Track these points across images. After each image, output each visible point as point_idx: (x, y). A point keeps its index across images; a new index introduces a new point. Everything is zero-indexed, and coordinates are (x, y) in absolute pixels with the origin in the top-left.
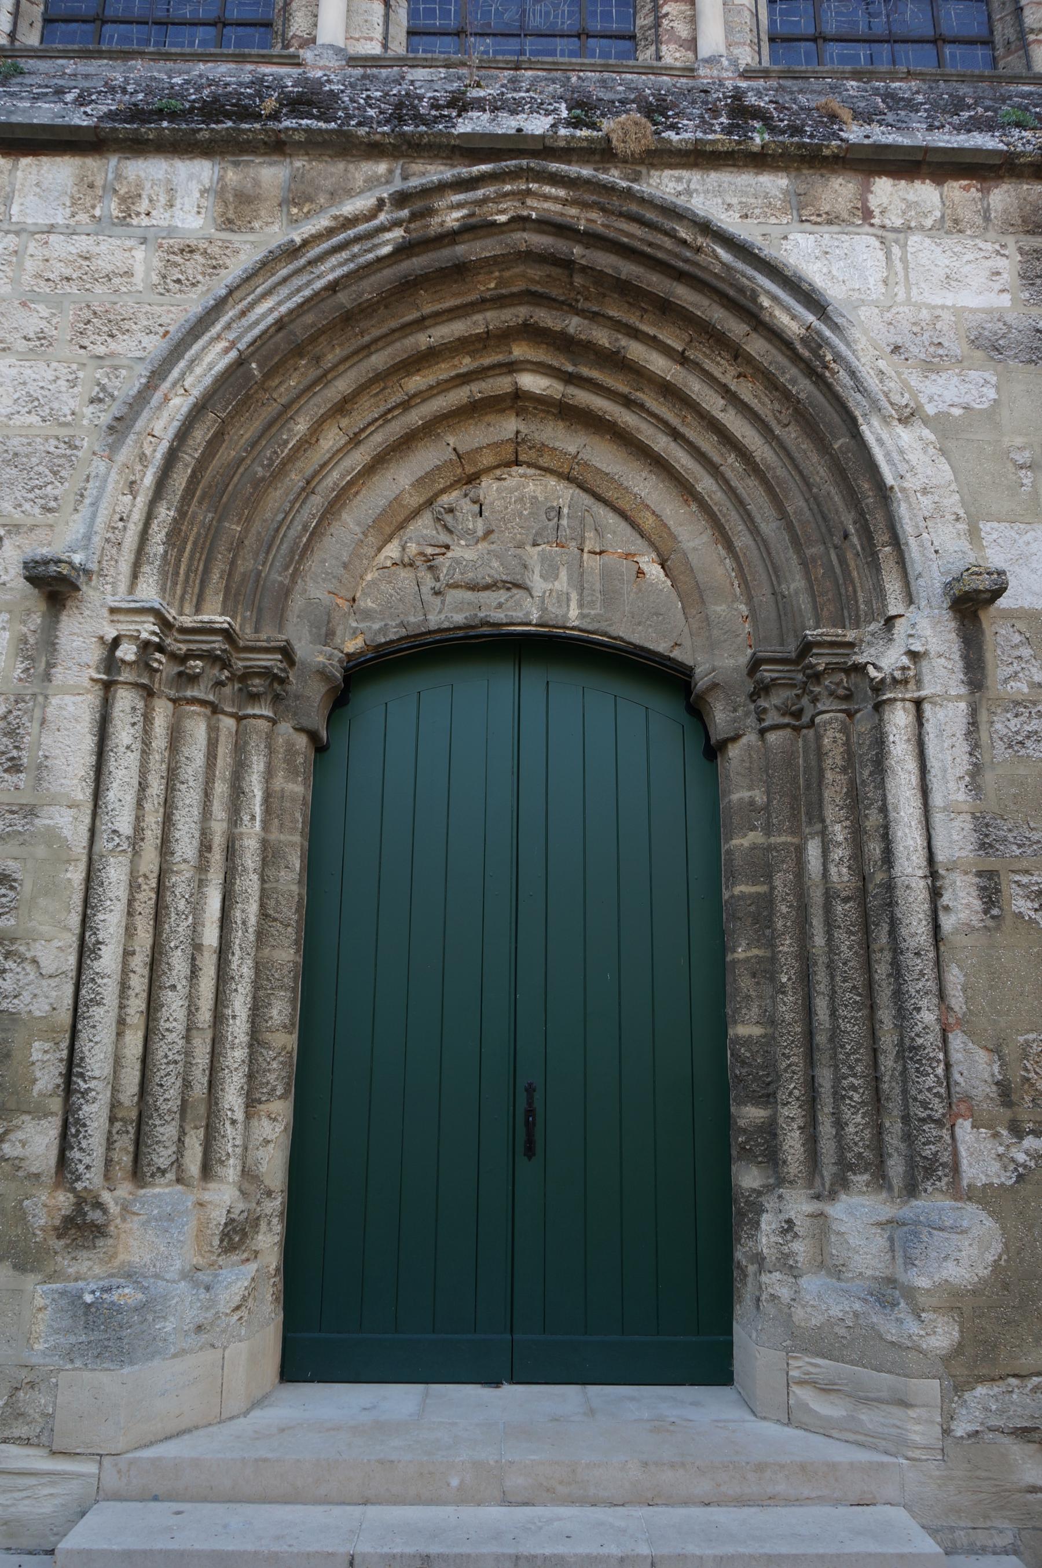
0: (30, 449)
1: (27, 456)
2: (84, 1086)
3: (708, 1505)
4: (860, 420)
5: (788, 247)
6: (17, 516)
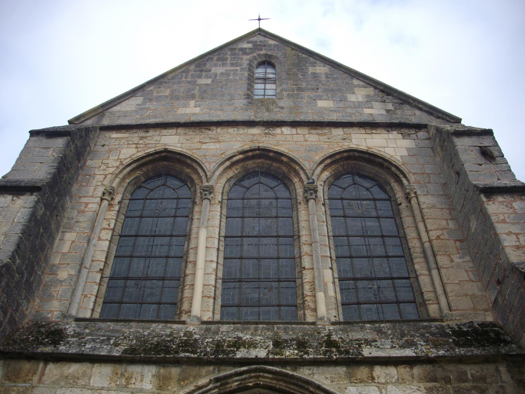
5: (347, 392)
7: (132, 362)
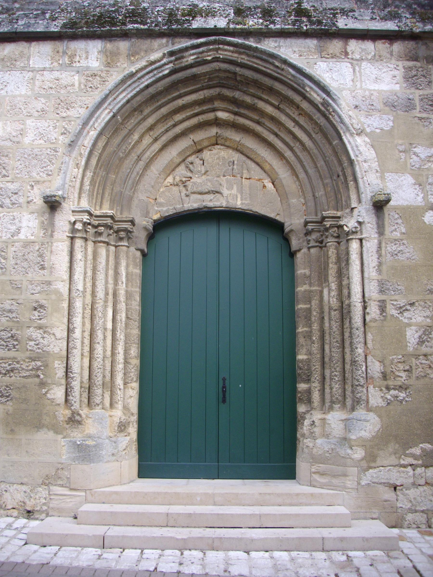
0: (41, 153)
1: (40, 155)
2: (72, 376)
3: (280, 506)
4: (342, 134)
6: (38, 178)
7: (74, 37)
